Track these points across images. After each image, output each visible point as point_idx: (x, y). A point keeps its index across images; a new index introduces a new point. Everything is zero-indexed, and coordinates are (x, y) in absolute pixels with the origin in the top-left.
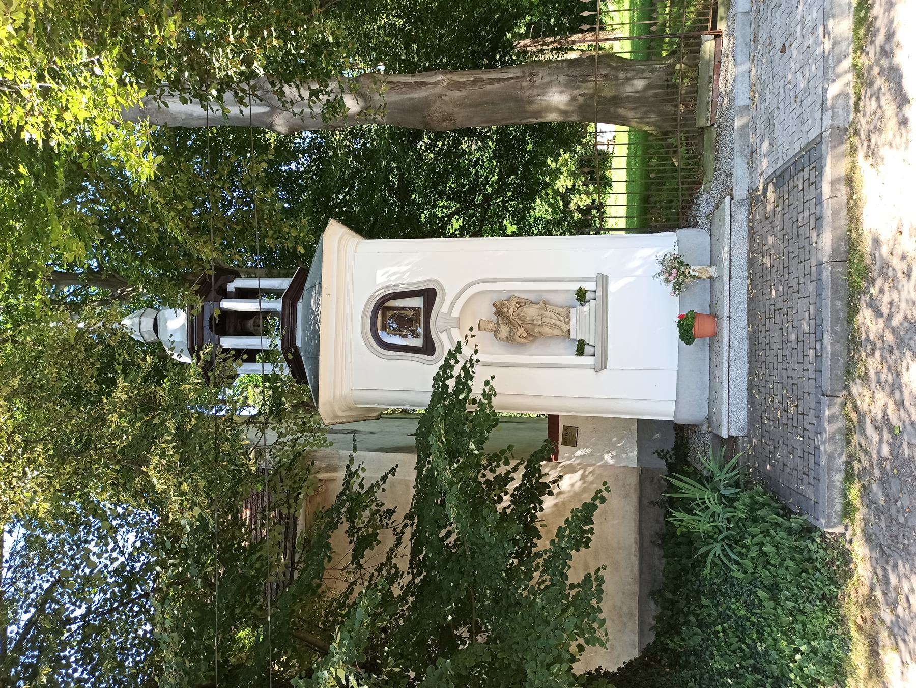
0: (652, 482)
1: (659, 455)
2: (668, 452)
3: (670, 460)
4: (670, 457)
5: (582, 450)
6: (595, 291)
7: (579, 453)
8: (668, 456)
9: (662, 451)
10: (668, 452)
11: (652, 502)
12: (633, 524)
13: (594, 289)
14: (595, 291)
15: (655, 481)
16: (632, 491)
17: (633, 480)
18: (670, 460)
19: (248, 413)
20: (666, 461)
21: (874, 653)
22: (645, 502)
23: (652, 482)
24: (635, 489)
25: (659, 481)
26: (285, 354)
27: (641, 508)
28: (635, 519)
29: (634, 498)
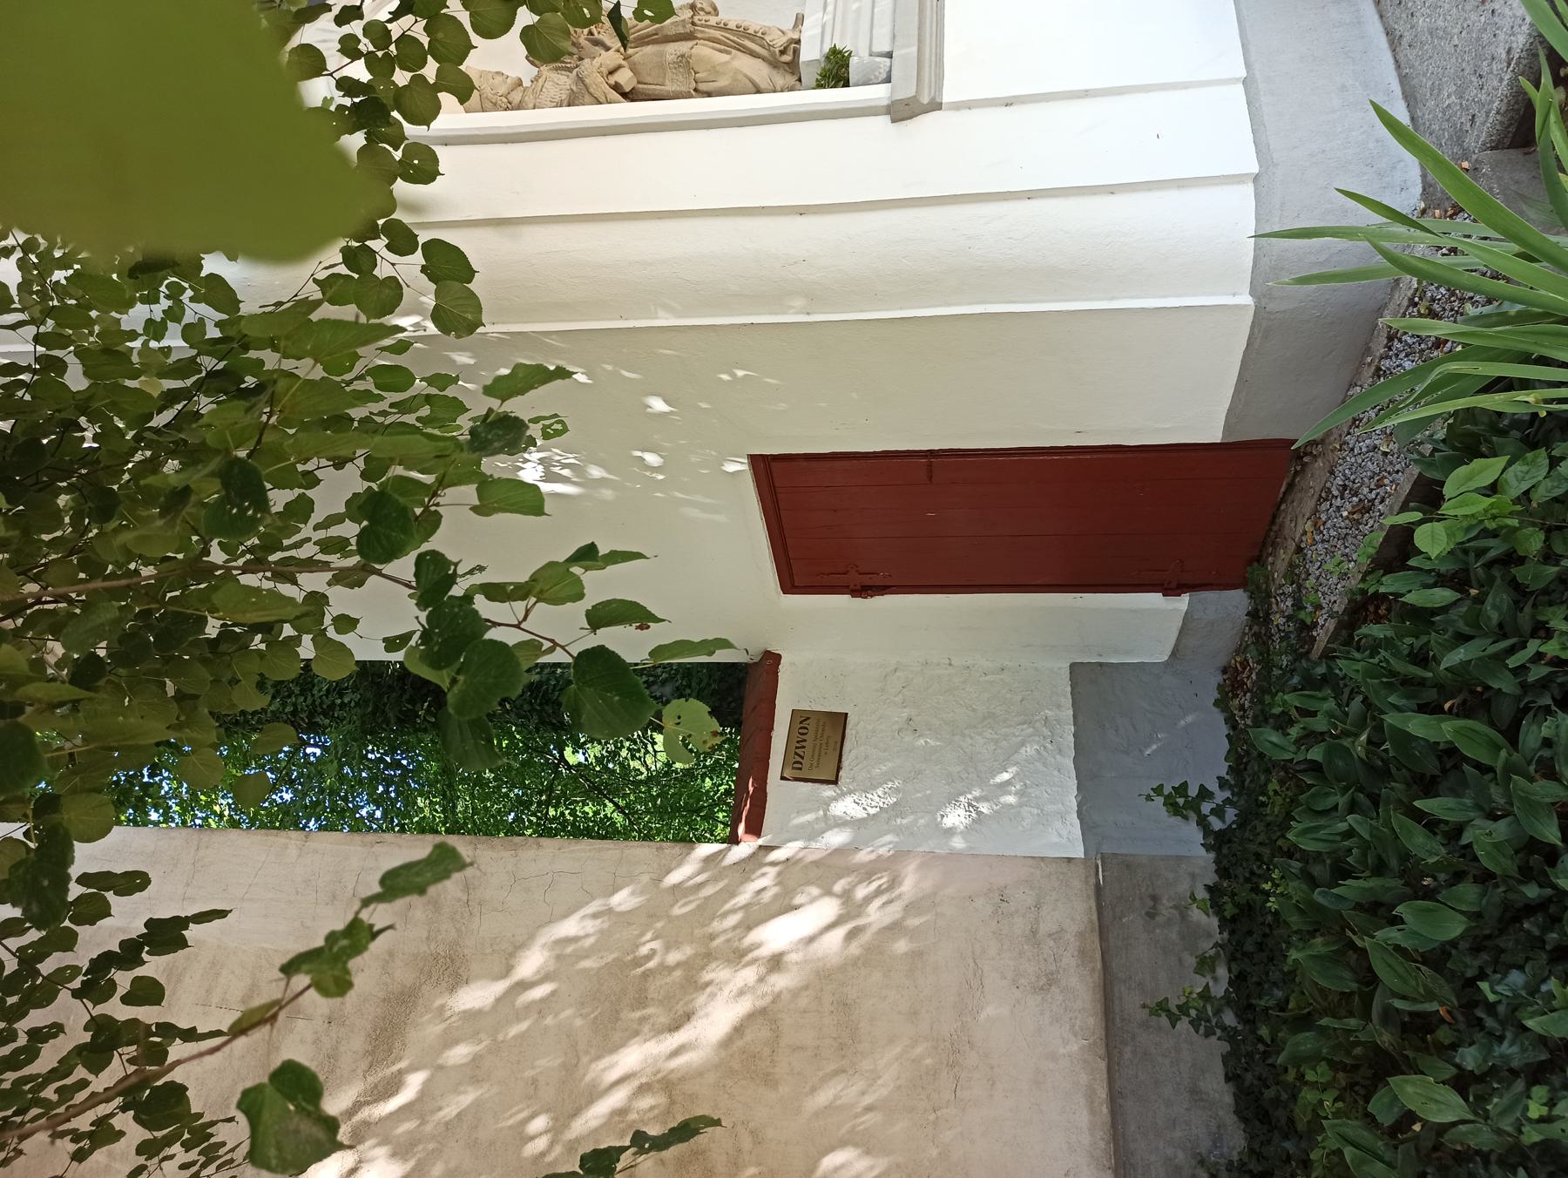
0: (1151, 915)
1: (1173, 808)
2: (1204, 794)
3: (1217, 824)
4: (1218, 812)
5: (594, 1124)
6: (890, 55)
7: (847, 807)
8: (1206, 808)
9: (1182, 789)
10: (1204, 794)
11: (1162, 1007)
12: (1083, 1118)
13: (887, 49)
14: (890, 55)
15: (1166, 910)
16: (1069, 960)
17: (1071, 913)
18: (1217, 824)
19: (1331, 625)
20: (1202, 822)
21: (1401, 977)
22: (1131, 1003)
23: (1151, 915)
24: (1082, 953)
25: (1183, 912)
26: (254, 522)
27: (1113, 1036)
28: (1090, 1095)
29: (1080, 987)
